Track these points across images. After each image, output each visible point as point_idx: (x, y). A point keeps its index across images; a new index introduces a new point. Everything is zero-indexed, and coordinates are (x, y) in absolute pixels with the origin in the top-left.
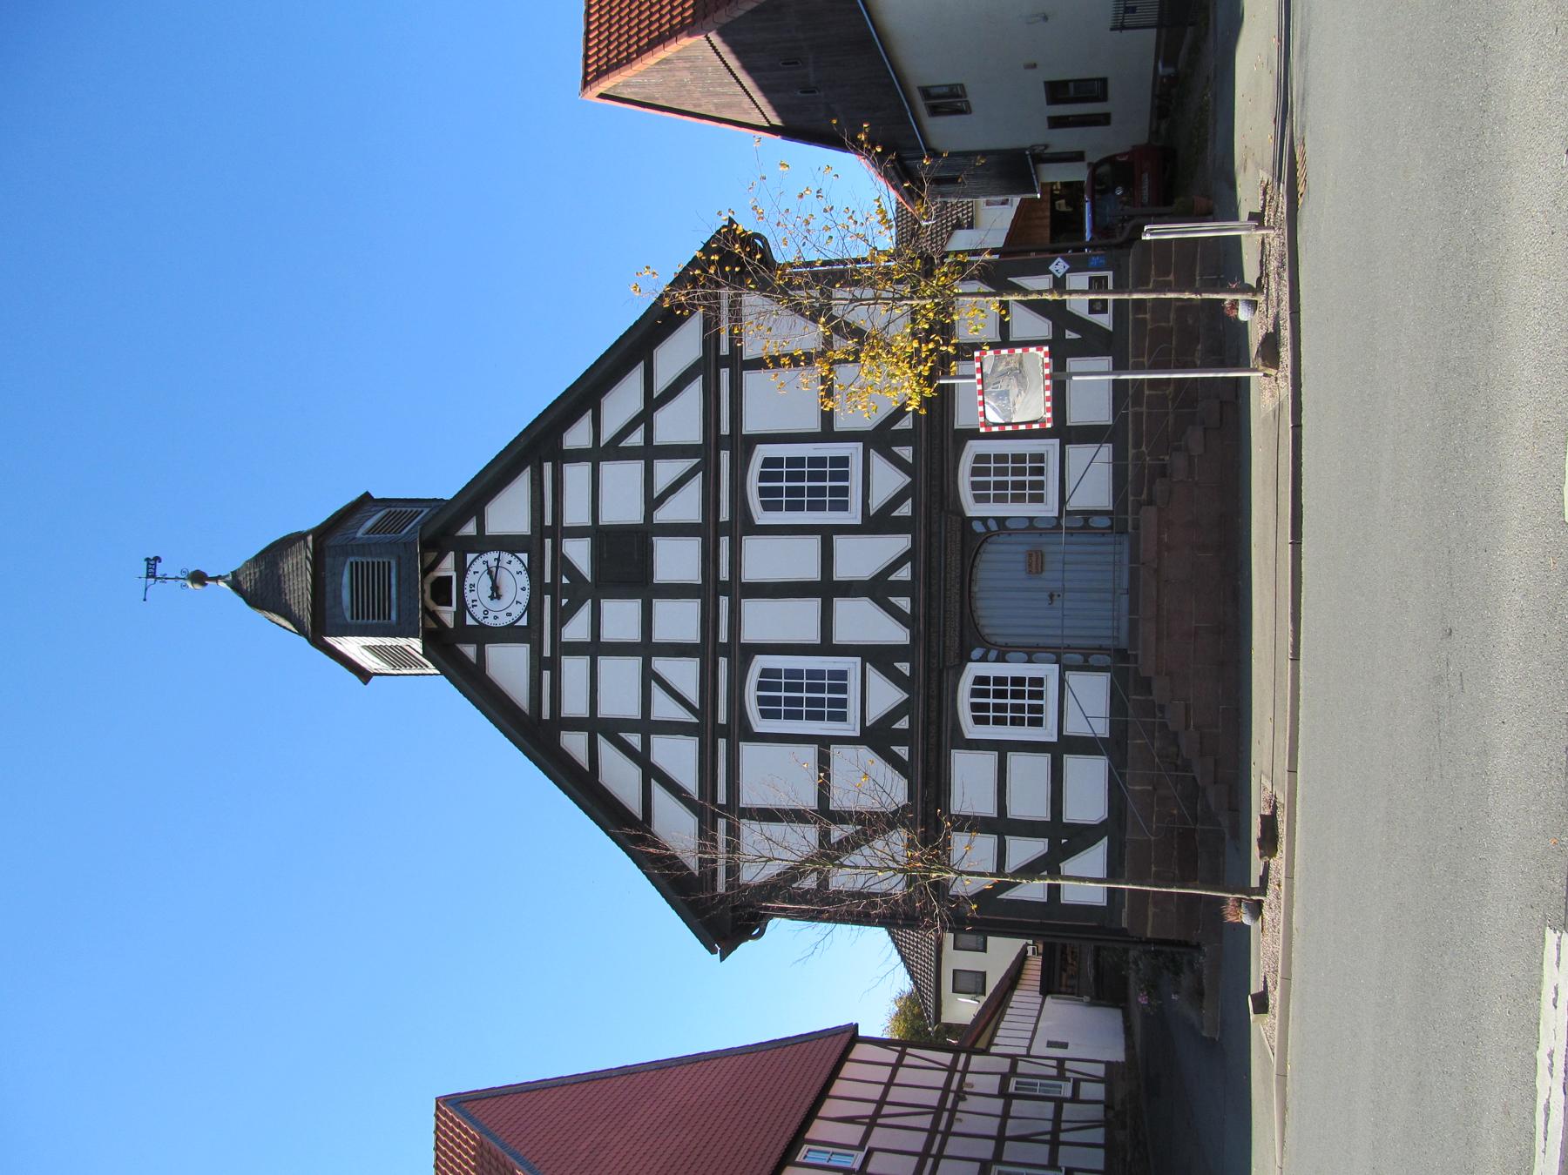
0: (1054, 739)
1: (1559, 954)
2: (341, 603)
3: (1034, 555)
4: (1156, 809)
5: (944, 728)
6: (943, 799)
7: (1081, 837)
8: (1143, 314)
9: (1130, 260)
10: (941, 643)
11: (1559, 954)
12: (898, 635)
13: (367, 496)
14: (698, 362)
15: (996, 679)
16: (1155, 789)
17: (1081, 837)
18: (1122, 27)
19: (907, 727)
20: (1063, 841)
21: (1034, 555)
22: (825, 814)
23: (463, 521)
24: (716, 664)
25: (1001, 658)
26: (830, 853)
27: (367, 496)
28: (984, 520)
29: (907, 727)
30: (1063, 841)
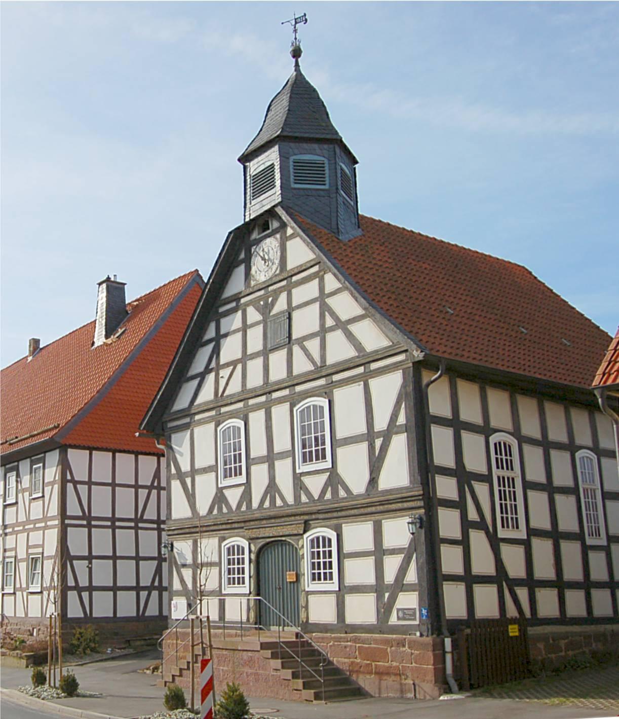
12: (255, 504)
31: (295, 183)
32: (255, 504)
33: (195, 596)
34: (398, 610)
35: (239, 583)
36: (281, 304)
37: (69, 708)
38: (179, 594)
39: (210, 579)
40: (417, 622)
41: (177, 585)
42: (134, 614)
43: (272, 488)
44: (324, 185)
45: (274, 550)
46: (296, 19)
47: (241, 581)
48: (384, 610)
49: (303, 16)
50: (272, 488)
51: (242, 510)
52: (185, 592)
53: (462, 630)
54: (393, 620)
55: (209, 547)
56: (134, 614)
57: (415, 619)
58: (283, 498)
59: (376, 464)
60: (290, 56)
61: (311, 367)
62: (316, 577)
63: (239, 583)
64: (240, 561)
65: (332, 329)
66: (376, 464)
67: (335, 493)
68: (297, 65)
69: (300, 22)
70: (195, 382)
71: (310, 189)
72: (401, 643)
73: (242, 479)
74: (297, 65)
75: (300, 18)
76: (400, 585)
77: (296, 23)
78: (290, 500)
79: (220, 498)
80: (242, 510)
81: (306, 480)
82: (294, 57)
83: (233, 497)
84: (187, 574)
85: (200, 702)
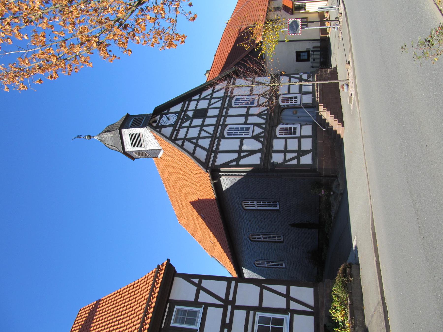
0: (299, 136)
1: (315, 21)
2: (129, 124)
3: (295, 111)
4: (324, 145)
5: (272, 136)
6: (271, 148)
7: (306, 152)
8: (322, 158)
9: (318, 288)
10: (273, 122)
11: (315, 21)
12: (264, 121)
13: (128, 115)
14: (214, 93)
15: (283, 135)
16: (324, 141)
17: (306, 152)
18: (313, 68)
19: (263, 135)
20: (301, 153)
21: (295, 111)
22: (240, 151)
23: (165, 110)
24: (218, 127)
25: (287, 124)
26: (240, 158)
27: (128, 115)
28: (284, 105)
29: (263, 135)
30: (301, 153)
32: (264, 121)
33: (301, 153)
35: (297, 99)
37: (356, 80)
38: (299, 161)
39: (293, 144)
41: (294, 162)
42: (312, 318)
43: (259, 115)
45: (283, 121)
47: (295, 129)
50: (259, 115)
52: (298, 158)
55: (278, 144)
56: (312, 318)
58: (261, 133)
61: (209, 140)
62: (296, 101)
63: (297, 99)
64: (286, 129)
65: (197, 141)
79: (256, 137)
81: (255, 133)
83: (258, 130)
84: (290, 156)
85: (347, 90)
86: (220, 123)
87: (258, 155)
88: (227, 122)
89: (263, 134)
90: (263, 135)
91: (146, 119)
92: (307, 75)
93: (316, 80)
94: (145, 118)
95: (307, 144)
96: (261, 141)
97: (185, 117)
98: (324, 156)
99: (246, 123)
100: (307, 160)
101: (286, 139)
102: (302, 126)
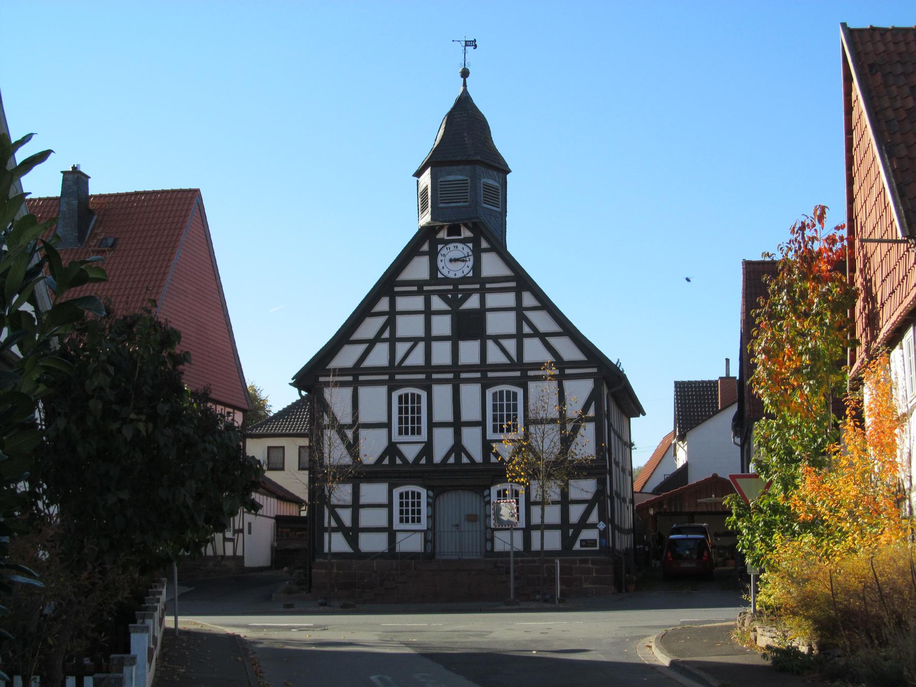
12: (438, 457)
22: (356, 425)
31: (484, 203)
34: (582, 541)
36: (473, 303)
40: (598, 548)
43: (458, 448)
44: (498, 207)
46: (466, 41)
48: (567, 542)
49: (473, 41)
50: (458, 448)
51: (384, 463)
52: (341, 528)
53: (868, 519)
54: (577, 546)
55: (374, 492)
57: (596, 546)
58: (469, 456)
59: (566, 441)
60: (459, 75)
66: (566, 441)
67: (458, 458)
68: (465, 85)
69: (470, 46)
70: (362, 348)
71: (491, 210)
72: (585, 561)
73: (424, 437)
74: (465, 85)
75: (470, 41)
76: (583, 524)
77: (466, 45)
78: (478, 458)
80: (384, 463)
82: (462, 77)
86: (488, 373)
87: (348, 460)
88: (436, 388)
89: (401, 463)
90: (398, 461)
91: (496, 211)
92: (596, 540)
93: (335, 564)
94: (499, 210)
95: (373, 543)
96: (383, 460)
97: (450, 296)
98: (341, 572)
99: (431, 425)
100: (338, 543)
101: (390, 506)
102: (495, 532)
